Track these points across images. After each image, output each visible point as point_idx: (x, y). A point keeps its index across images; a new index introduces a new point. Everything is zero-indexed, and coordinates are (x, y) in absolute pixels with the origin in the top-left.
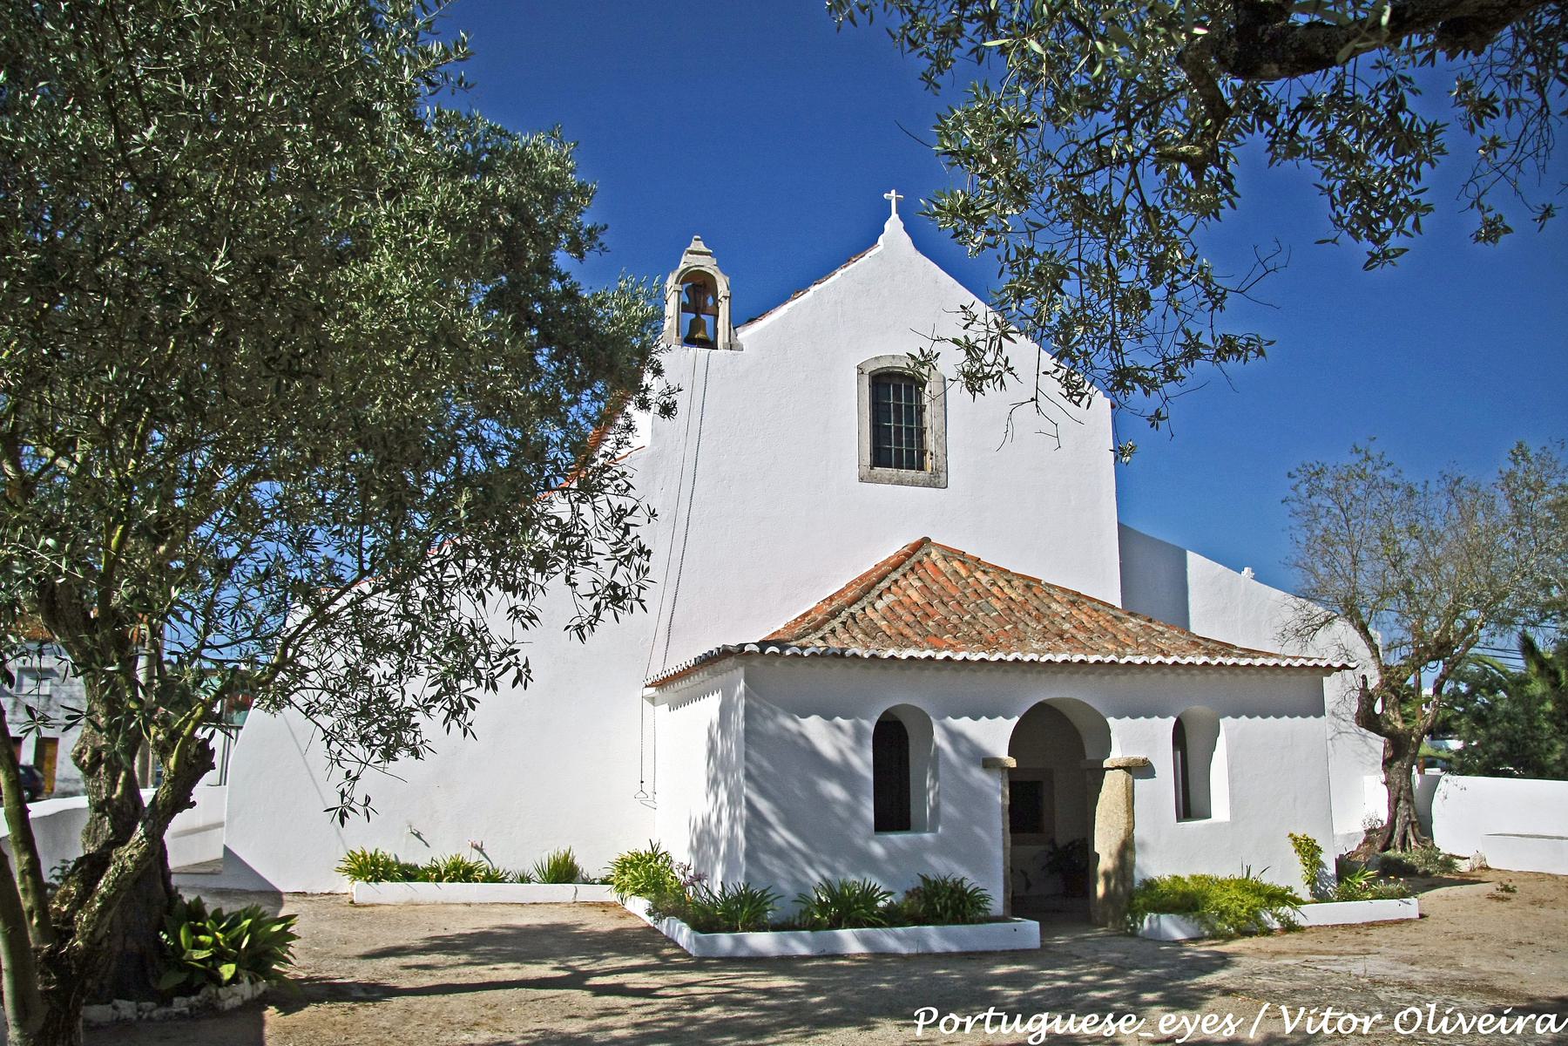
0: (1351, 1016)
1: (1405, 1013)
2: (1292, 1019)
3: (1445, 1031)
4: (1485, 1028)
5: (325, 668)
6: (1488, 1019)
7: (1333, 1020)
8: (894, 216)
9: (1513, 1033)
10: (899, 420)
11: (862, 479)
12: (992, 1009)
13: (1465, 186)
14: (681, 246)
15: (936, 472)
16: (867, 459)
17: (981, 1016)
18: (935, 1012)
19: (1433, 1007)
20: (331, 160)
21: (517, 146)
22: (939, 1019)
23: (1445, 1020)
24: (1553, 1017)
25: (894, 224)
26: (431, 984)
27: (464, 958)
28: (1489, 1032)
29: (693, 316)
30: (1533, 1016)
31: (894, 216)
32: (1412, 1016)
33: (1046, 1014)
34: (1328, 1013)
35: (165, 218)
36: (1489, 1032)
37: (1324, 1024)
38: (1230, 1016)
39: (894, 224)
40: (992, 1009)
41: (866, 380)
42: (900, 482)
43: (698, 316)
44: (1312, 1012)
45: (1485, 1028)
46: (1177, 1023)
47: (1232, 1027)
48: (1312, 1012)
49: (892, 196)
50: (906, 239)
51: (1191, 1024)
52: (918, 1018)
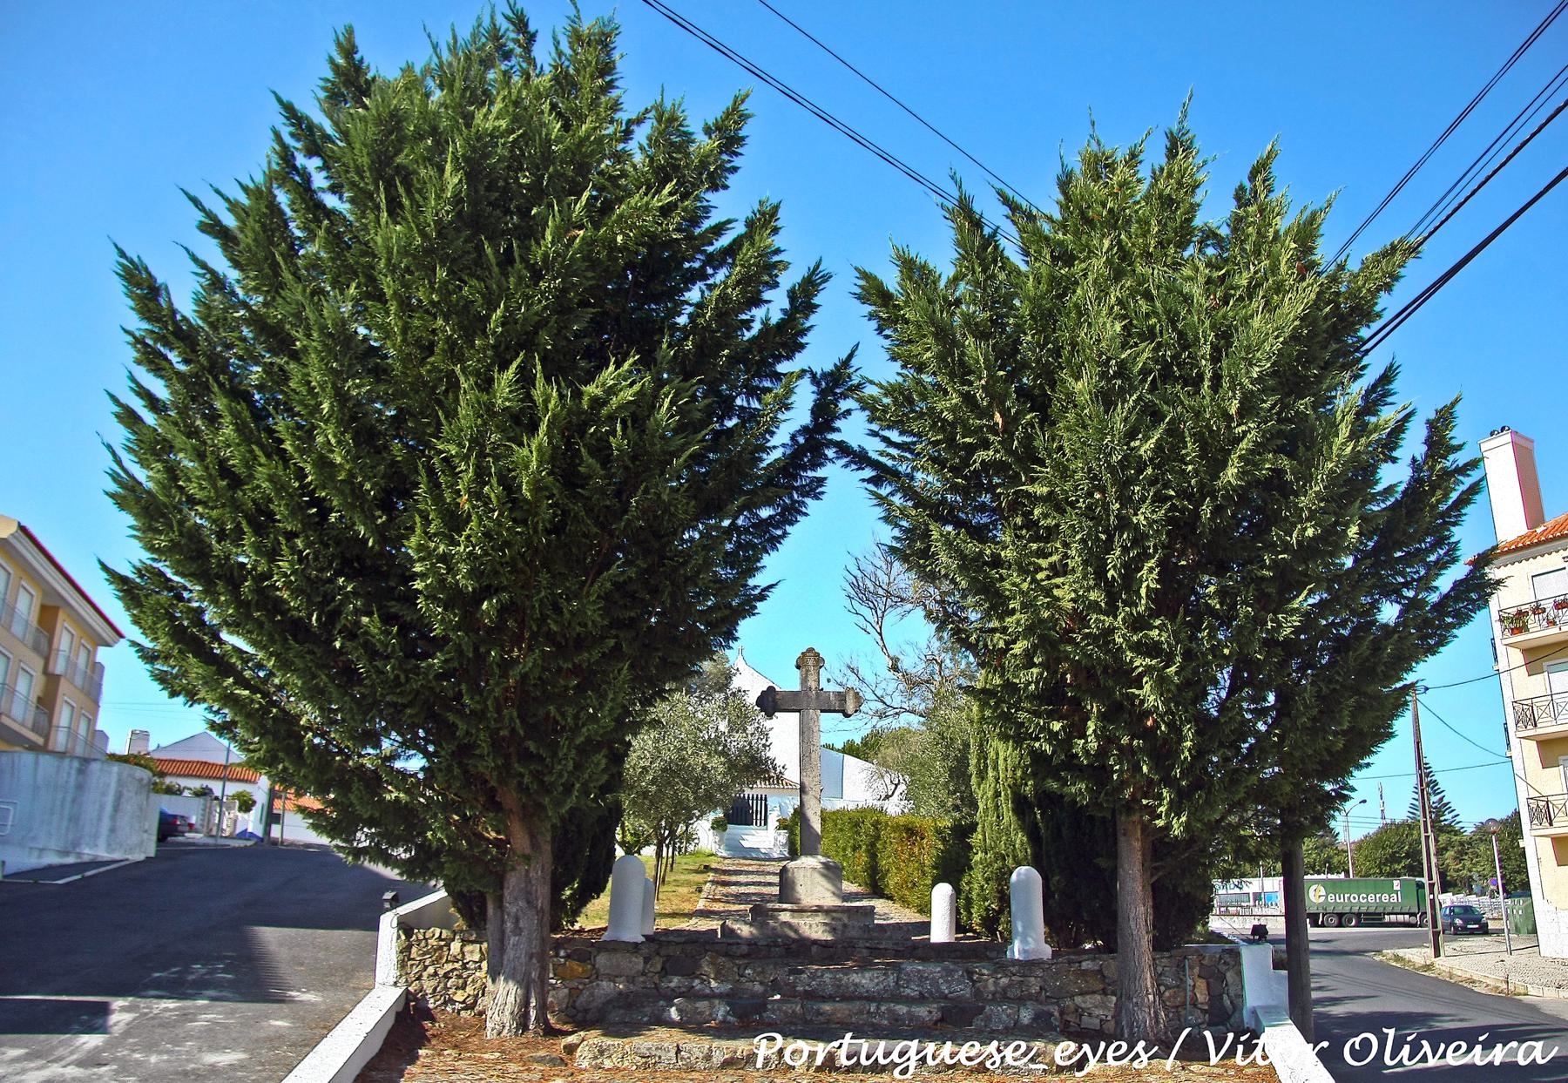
1: (1357, 1040)
5: (236, 482)
6: (1118, 1048)
19: (1391, 1032)
21: (248, 245)
23: (1407, 1049)
27: (42, 1062)
28: (972, 1063)
30: (1514, 1044)
32: (1366, 1044)
33: (916, 1042)
36: (972, 1063)
38: (1142, 1044)
40: (849, 1035)
44: (1242, 1039)
45: (1116, 1059)
46: (1075, 1053)
48: (1242, 1039)
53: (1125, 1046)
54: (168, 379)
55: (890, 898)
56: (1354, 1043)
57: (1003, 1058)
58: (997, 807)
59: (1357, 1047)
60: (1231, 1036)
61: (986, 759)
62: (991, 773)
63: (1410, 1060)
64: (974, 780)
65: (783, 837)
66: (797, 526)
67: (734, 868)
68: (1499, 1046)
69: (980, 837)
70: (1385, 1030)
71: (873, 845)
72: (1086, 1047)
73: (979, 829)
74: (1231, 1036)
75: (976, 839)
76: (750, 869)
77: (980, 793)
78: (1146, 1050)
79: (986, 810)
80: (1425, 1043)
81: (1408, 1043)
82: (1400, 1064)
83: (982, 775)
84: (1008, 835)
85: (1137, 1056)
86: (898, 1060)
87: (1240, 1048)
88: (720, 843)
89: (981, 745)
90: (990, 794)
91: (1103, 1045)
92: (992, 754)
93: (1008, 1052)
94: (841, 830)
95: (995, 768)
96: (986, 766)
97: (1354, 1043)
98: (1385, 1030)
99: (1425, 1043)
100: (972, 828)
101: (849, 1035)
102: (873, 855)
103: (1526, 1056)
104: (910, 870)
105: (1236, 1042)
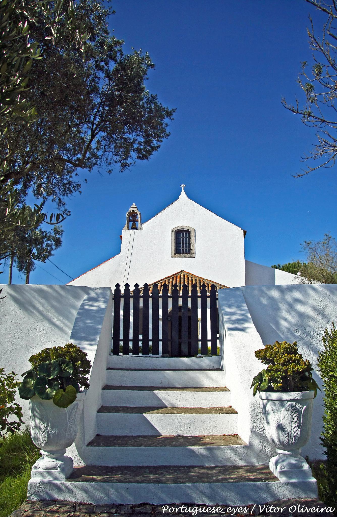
2: (262, 508)
6: (313, 509)
7: (272, 510)
8: (183, 191)
10: (183, 242)
11: (172, 257)
12: (183, 506)
14: (130, 206)
15: (192, 254)
16: (174, 252)
17: (180, 508)
19: (299, 505)
20: (91, 14)
22: (169, 509)
23: (302, 509)
24: (331, 508)
25: (183, 193)
29: (133, 222)
30: (325, 508)
31: (183, 191)
32: (294, 508)
34: (272, 507)
37: (270, 510)
38: (246, 508)
39: (183, 193)
41: (174, 233)
42: (183, 257)
43: (134, 222)
47: (246, 511)
49: (182, 186)
50: (186, 196)
53: (315, 508)
54: (220, 479)
57: (216, 511)
66: (275, 265)
68: (322, 508)
72: (234, 509)
78: (247, 509)
80: (306, 508)
85: (245, 510)
86: (193, 511)
93: (217, 510)
99: (306, 508)
103: (328, 511)
105: (266, 507)
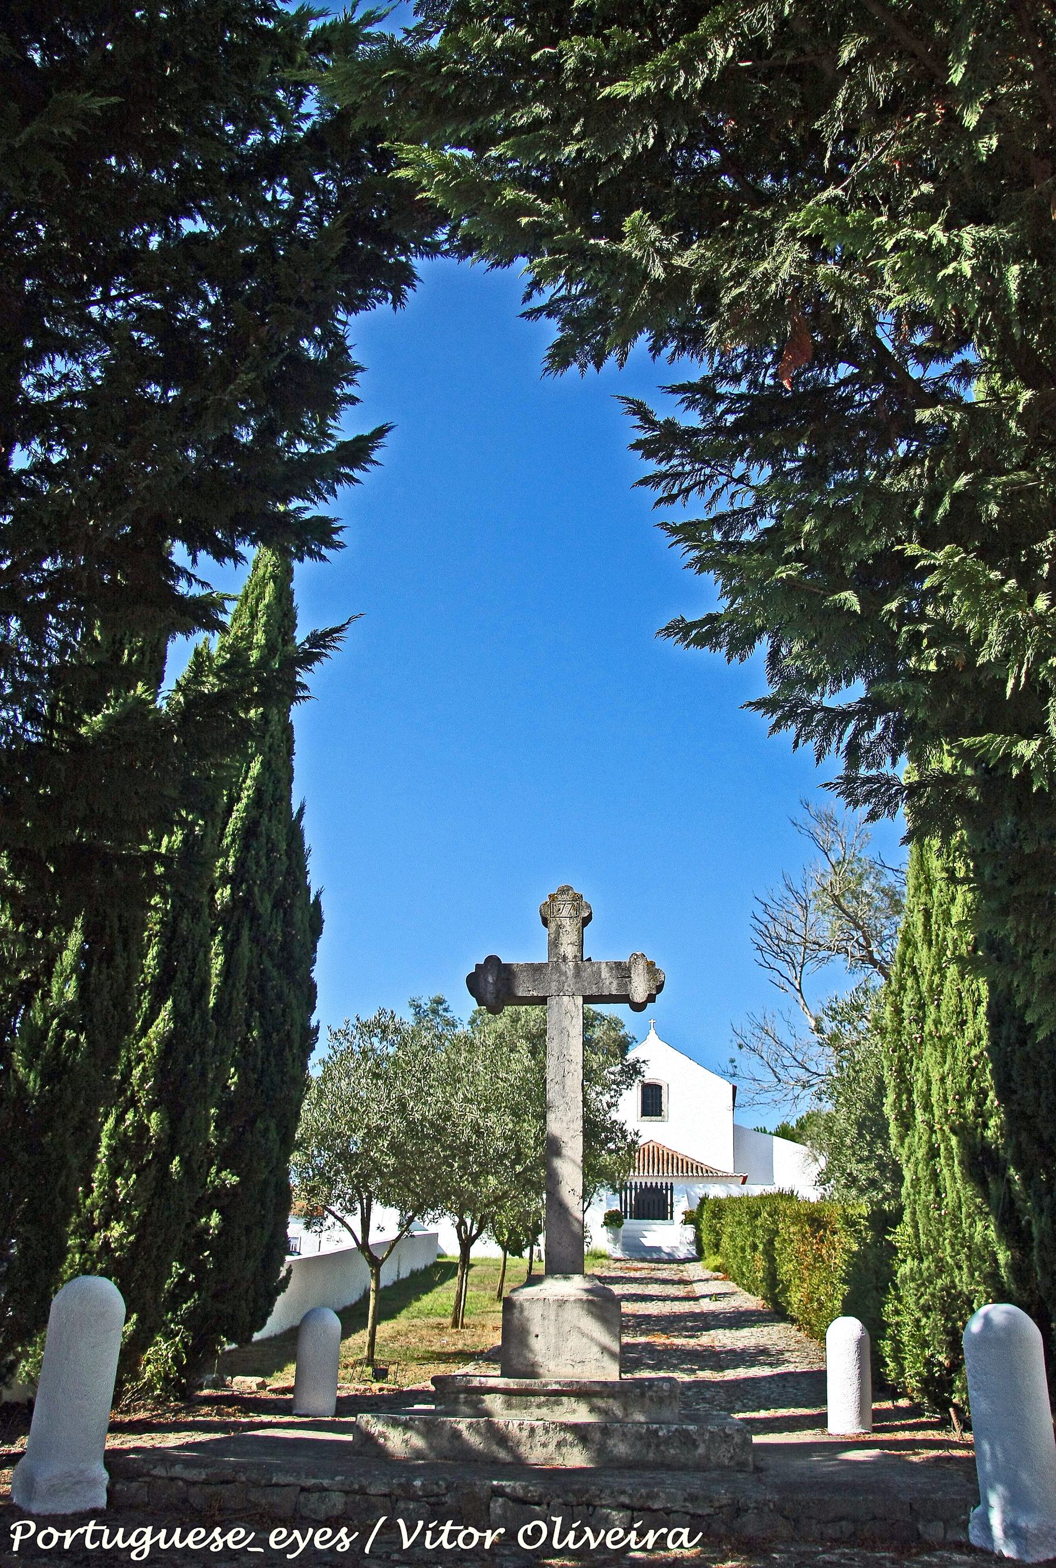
0: (471, 1530)
1: (530, 1527)
3: (572, 1546)
4: (614, 1543)
6: (324, 1534)
7: (453, 1536)
9: (644, 1549)
13: (651, 998)
18: (33, 1526)
19: (559, 1520)
24: (686, 1532)
26: (826, 1440)
32: (537, 1530)
34: (448, 1527)
35: (758, 282)
37: (444, 1538)
38: (344, 1530)
40: (450, 1522)
44: (431, 1526)
45: (614, 1543)
46: (622, 1539)
47: (347, 1542)
48: (431, 1526)
51: (304, 1539)
52: (14, 1532)
53: (285, 1532)
55: (793, 1321)
56: (526, 1530)
57: (225, 1543)
58: (935, 1176)
59: (529, 1533)
60: (421, 1523)
61: (910, 1093)
62: (920, 1115)
63: (689, 1542)
64: (893, 1129)
65: (689, 1232)
67: (620, 1274)
68: (652, 1532)
69: (910, 1230)
70: (553, 1518)
71: (771, 1242)
72: (296, 1533)
73: (907, 1217)
74: (421, 1523)
75: (901, 1235)
76: (637, 1274)
77: (904, 1152)
79: (916, 1182)
80: (587, 1529)
81: (573, 1529)
82: (681, 1546)
83: (906, 1121)
84: (956, 1226)
86: (134, 1544)
87: (429, 1534)
88: (615, 1240)
89: (901, 1070)
90: (921, 1153)
91: (311, 1531)
92: (920, 1084)
94: (739, 1223)
95: (928, 1107)
96: (911, 1106)
97: (526, 1530)
98: (553, 1518)
99: (587, 1529)
100: (896, 1218)
101: (93, 1522)
102: (771, 1260)
104: (815, 1281)
105: (425, 1528)
